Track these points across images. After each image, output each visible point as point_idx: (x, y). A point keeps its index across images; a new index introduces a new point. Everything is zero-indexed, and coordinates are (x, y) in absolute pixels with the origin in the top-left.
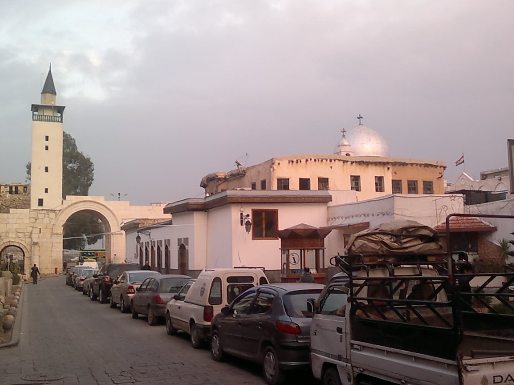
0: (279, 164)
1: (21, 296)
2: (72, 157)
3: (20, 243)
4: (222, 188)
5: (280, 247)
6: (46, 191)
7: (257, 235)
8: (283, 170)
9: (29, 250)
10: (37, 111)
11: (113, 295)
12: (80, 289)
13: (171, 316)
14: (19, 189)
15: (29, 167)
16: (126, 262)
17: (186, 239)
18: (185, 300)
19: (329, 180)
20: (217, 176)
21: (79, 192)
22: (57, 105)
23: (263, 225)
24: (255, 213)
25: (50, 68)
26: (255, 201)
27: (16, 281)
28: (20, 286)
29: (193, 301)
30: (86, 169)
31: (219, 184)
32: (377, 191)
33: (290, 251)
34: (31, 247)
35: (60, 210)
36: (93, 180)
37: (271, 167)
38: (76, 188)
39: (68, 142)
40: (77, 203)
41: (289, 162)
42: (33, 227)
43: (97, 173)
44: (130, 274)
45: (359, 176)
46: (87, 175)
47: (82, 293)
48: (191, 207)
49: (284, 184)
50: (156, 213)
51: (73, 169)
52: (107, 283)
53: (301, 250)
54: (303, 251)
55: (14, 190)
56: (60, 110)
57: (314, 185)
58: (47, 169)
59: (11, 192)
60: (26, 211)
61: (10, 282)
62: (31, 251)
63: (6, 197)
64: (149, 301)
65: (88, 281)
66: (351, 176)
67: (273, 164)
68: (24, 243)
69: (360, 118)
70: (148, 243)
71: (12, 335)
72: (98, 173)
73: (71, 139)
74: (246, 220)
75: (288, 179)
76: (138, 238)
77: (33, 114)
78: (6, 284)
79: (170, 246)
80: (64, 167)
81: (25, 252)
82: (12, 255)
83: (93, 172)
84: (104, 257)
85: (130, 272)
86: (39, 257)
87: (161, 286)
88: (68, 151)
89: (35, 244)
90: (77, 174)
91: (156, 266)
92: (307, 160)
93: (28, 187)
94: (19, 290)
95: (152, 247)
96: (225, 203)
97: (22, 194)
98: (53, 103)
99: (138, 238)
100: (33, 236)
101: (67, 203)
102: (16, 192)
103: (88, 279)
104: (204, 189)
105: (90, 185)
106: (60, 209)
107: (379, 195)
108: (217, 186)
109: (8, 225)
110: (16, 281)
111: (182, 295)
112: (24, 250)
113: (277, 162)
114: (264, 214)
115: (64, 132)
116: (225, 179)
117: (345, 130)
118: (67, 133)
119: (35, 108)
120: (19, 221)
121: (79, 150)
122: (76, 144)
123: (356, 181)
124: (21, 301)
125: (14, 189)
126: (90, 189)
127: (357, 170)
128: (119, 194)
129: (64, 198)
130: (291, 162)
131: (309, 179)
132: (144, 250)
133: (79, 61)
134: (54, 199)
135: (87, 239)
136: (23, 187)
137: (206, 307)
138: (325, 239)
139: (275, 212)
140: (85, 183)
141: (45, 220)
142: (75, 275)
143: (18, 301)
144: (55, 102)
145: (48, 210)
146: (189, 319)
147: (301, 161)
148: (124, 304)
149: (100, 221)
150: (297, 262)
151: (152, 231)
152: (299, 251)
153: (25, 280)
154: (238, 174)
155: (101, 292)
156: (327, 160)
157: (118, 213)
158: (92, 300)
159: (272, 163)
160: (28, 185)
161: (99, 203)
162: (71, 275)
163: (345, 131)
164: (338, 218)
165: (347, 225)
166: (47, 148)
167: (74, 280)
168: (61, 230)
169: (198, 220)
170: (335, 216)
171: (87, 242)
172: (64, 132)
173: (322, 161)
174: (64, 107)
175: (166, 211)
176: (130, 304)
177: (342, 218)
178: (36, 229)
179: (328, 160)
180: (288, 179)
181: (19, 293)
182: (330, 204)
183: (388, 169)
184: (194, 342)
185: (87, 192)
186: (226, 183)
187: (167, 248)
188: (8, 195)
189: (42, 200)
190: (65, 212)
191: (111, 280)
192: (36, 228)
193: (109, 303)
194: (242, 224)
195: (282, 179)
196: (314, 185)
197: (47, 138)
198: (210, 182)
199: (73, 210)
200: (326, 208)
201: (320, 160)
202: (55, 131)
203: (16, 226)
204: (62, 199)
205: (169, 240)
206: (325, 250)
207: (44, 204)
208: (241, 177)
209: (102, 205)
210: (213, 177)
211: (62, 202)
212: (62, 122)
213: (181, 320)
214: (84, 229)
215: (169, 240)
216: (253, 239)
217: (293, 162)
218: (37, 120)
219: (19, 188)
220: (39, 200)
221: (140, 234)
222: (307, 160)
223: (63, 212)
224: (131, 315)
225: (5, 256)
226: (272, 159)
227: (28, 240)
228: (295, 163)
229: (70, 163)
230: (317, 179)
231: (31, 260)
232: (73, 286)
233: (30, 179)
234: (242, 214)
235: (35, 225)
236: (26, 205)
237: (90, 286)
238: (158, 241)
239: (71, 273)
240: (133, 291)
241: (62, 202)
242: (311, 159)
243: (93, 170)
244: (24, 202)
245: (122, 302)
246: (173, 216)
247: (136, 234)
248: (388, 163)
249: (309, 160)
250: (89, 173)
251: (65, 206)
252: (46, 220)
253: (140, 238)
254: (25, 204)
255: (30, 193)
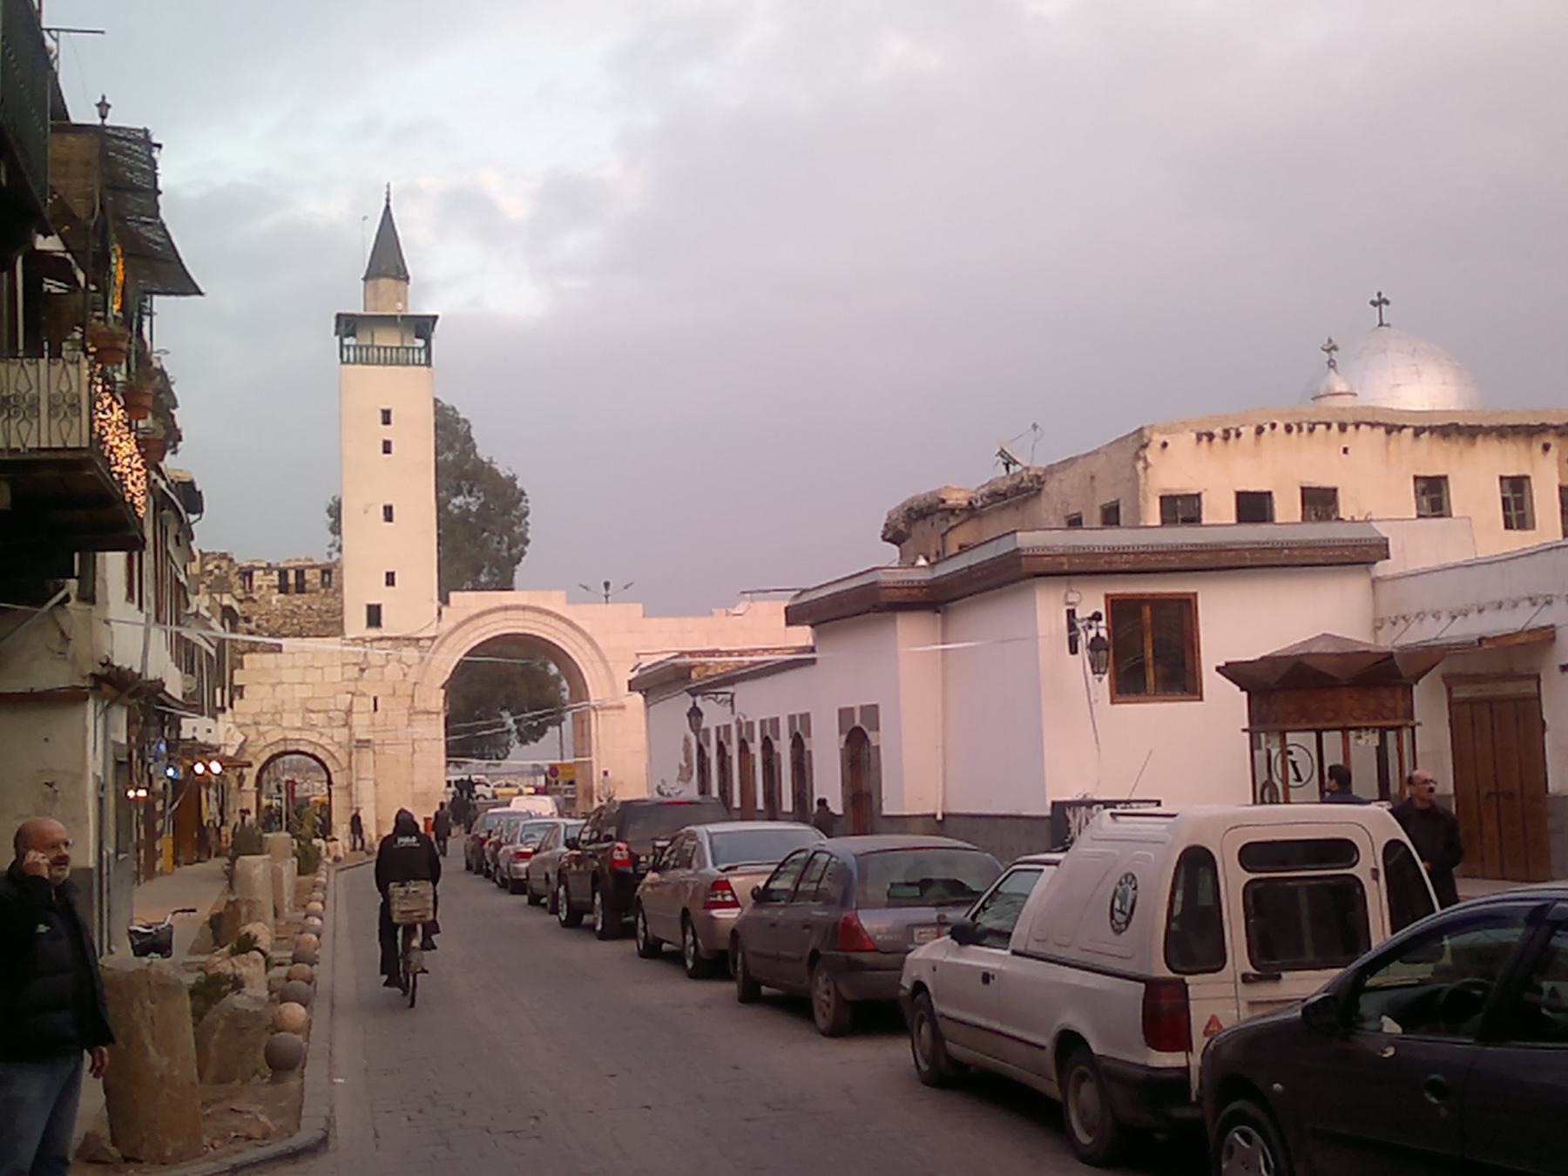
0: (1165, 445)
1: (328, 916)
2: (464, 476)
3: (316, 744)
4: (962, 541)
5: (1246, 726)
6: (390, 579)
7: (1130, 682)
8: (1178, 467)
9: (345, 764)
10: (354, 335)
11: (647, 911)
12: (516, 886)
13: (939, 1008)
14: (307, 577)
15: (335, 511)
16: (662, 794)
17: (871, 712)
18: (1012, 946)
19: (1340, 493)
20: (943, 501)
21: (487, 583)
22: (411, 313)
23: (1148, 653)
24: (1120, 608)
25: (388, 200)
26: (1114, 567)
27: (308, 862)
28: (323, 880)
29: (1062, 953)
30: (506, 512)
31: (951, 529)
32: (1508, 526)
33: (1289, 735)
34: (350, 755)
35: (433, 639)
36: (527, 542)
37: (1137, 457)
38: (478, 570)
39: (450, 431)
40: (482, 616)
41: (1199, 438)
42: (353, 694)
43: (538, 525)
44: (710, 835)
45: (1445, 478)
46: (509, 528)
47: (525, 899)
48: (885, 597)
49: (1181, 508)
50: (763, 629)
51: (465, 511)
52: (621, 869)
53: (1383, 731)
54: (1391, 735)
55: (292, 582)
56: (423, 326)
57: (1287, 508)
58: (388, 513)
59: (283, 588)
60: (332, 644)
61: (289, 867)
62: (350, 767)
63: (269, 602)
64: (814, 942)
65: (543, 861)
66: (1416, 478)
67: (1145, 446)
68: (327, 739)
69: (1380, 302)
70: (728, 727)
71: (302, 1089)
72: (543, 522)
73: (458, 421)
74: (1092, 633)
75: (1198, 496)
76: (695, 713)
77: (342, 345)
78: (276, 877)
79: (809, 735)
80: (441, 506)
81: (331, 770)
82: (293, 782)
83: (528, 519)
84: (571, 783)
85: (712, 828)
86: (376, 785)
87: (863, 875)
88: (451, 457)
89: (364, 744)
90: (480, 528)
91: (760, 805)
92: (1260, 430)
93: (335, 571)
94: (319, 894)
95: (720, 745)
96: (1011, 575)
97: (317, 592)
98: (400, 306)
99: (695, 713)
100: (356, 719)
101: (452, 615)
102: (301, 588)
103: (545, 854)
104: (895, 547)
105: (519, 561)
106: (432, 634)
107: (1518, 540)
108: (944, 535)
109: (278, 688)
110: (308, 862)
111: (987, 921)
112: (328, 764)
113: (1158, 439)
114: (1147, 611)
115: (436, 401)
116: (971, 511)
117: (1335, 341)
118: (446, 402)
119: (347, 325)
120: (313, 676)
121: (483, 453)
122: (473, 435)
123: (1433, 495)
124: (326, 938)
125: (292, 579)
126: (520, 572)
127: (1435, 458)
128: (607, 585)
129: (444, 600)
130: (1205, 439)
131: (1270, 493)
132: (712, 752)
133: (467, 208)
134: (414, 604)
135: (514, 727)
136: (318, 571)
137: (1152, 985)
138: (1415, 688)
139: (1187, 604)
140: (505, 554)
141: (391, 669)
142: (494, 838)
143: (319, 936)
144: (405, 304)
145: (397, 638)
146: (1054, 1030)
147: (1238, 435)
148: (695, 943)
149: (553, 669)
150: (1305, 779)
151: (741, 691)
152: (1313, 735)
153: (337, 859)
154: (1017, 490)
155: (598, 900)
156: (1329, 426)
157: (609, 643)
158: (565, 924)
159: (1139, 443)
160: (334, 565)
161: (549, 613)
162: (483, 841)
163: (1335, 348)
164: (1420, 616)
165: (1475, 639)
166: (387, 447)
167: (494, 856)
168: (437, 701)
169: (911, 642)
170: (1404, 611)
171: (514, 736)
172: (436, 401)
173: (1311, 430)
174: (435, 318)
175: (793, 616)
176: (725, 946)
177: (1436, 616)
178: (364, 699)
179: (1335, 427)
180: (1198, 496)
181: (319, 906)
182: (1381, 568)
183: (1546, 448)
184: (1085, 1139)
185: (511, 581)
186: (973, 522)
187: (797, 743)
188: (276, 597)
189: (379, 607)
190: (450, 641)
191: (634, 859)
192: (363, 695)
193: (634, 936)
194: (1074, 650)
195: (1173, 498)
196: (1287, 508)
197: (386, 417)
198: (914, 523)
199: (471, 636)
200: (1369, 583)
201: (1305, 426)
202: (408, 392)
203: (301, 692)
204: (436, 603)
205: (806, 718)
206: (1417, 729)
207: (384, 622)
208: (1026, 500)
209: (560, 618)
210: (930, 507)
211: (440, 613)
212: (428, 364)
213: (999, 1033)
214: (507, 693)
215: (806, 718)
216: (1112, 702)
217: (1211, 436)
218: (355, 363)
219: (308, 575)
220: (370, 607)
221: (698, 699)
222: (1260, 430)
223: (442, 643)
224: (732, 988)
225: (273, 785)
226: (1141, 430)
227: (341, 735)
228: (1217, 440)
229: (456, 495)
230: (1299, 492)
231: (350, 795)
232: (488, 875)
233: (340, 550)
234: (1071, 614)
235: (362, 686)
236: (331, 625)
237: (553, 877)
238: (762, 722)
239: (484, 835)
240: (729, 898)
241: (440, 613)
242: (1273, 426)
243: (526, 514)
244: (325, 617)
245: (690, 938)
246: (818, 636)
247: (684, 702)
248: (1543, 429)
249: (1267, 427)
250: (513, 524)
251: (448, 623)
252: (393, 671)
253: (700, 714)
254: (326, 623)
255: (340, 589)
